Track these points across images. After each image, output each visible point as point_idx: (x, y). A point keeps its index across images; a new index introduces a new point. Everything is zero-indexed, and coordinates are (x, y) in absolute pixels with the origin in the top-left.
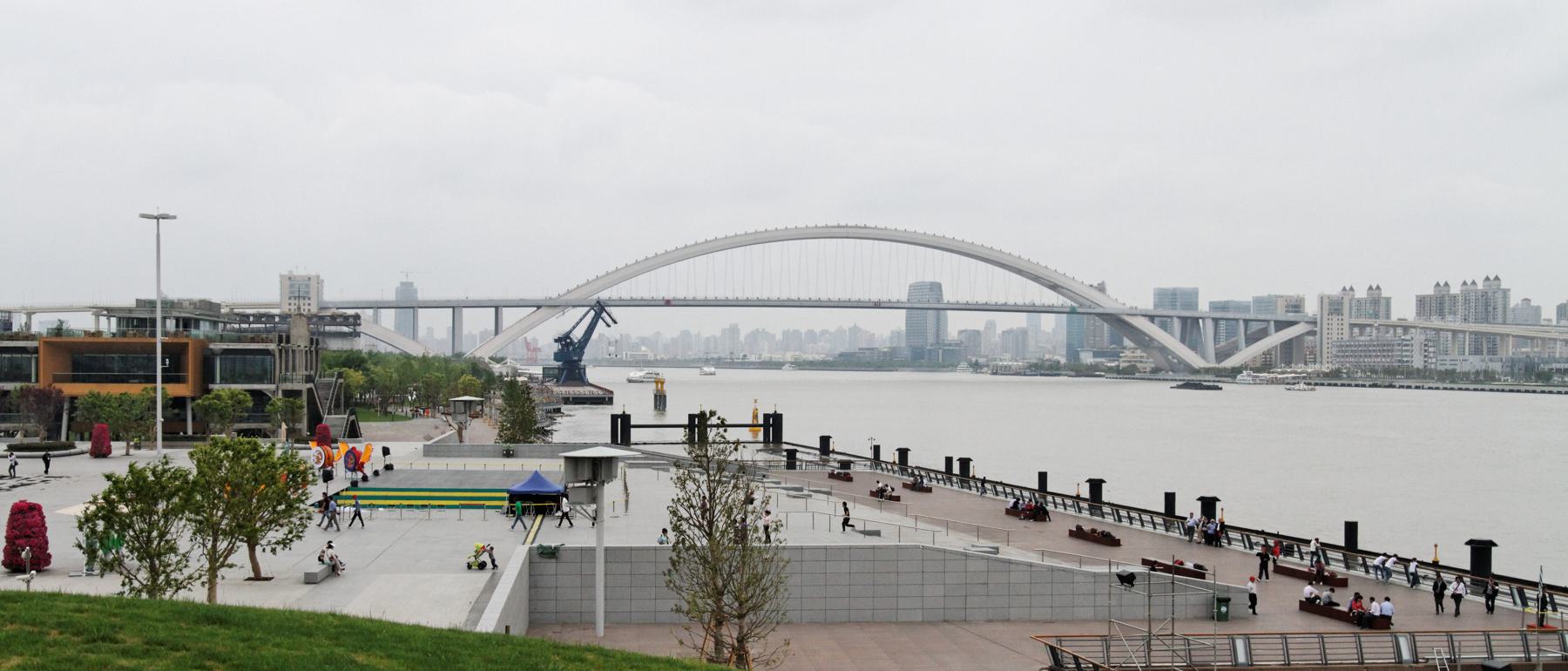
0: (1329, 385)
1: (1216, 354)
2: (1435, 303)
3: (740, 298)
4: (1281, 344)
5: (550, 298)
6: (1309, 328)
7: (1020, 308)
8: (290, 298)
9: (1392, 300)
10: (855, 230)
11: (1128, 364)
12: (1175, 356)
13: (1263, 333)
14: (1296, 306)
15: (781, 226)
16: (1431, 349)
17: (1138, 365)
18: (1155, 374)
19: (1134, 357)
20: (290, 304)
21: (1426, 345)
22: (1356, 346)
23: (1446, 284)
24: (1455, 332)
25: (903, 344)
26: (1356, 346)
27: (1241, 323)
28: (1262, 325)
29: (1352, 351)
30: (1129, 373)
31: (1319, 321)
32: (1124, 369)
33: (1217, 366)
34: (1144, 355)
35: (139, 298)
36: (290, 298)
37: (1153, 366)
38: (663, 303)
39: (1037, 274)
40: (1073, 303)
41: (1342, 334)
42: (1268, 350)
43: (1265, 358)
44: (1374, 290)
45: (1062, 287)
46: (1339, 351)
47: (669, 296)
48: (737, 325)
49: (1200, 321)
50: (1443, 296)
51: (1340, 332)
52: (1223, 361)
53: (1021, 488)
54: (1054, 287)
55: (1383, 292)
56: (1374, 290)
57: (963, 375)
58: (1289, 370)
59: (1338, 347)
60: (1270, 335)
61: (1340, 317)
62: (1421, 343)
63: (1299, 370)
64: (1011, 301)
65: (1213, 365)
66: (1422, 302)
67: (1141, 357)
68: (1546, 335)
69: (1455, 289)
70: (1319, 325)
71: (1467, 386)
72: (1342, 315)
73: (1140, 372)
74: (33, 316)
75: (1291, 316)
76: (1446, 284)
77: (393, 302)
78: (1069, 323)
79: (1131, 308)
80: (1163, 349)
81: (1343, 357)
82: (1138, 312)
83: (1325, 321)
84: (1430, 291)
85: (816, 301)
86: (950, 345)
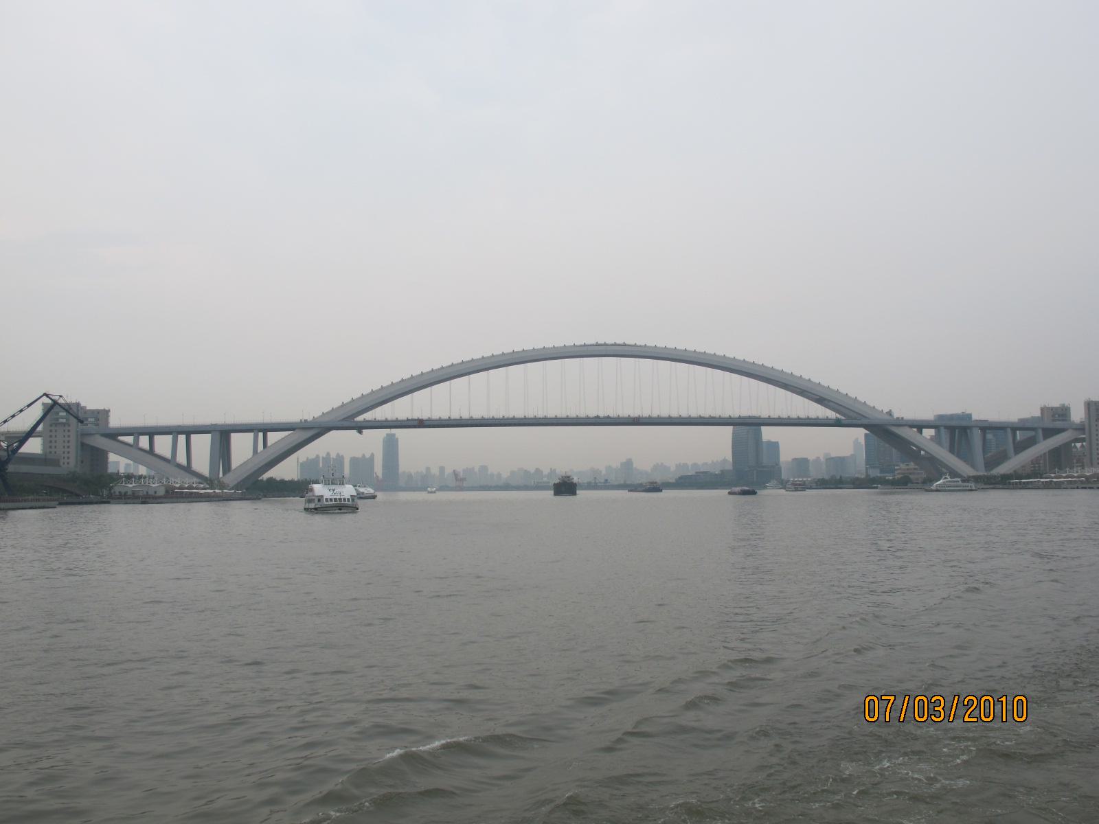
0: (1083, 488)
1: (985, 464)
3: (611, 415)
4: (1050, 451)
5: (306, 421)
8: (51, 426)
11: (901, 476)
13: (1031, 442)
17: (911, 477)
19: (908, 469)
20: (51, 431)
25: (729, 467)
27: (1009, 430)
28: (1031, 434)
31: (1087, 427)
33: (986, 474)
35: (111, 414)
36: (51, 426)
38: (416, 423)
40: (838, 416)
41: (68, 442)
43: (1034, 467)
45: (829, 401)
47: (425, 416)
52: (992, 469)
53: (152, 433)
54: (821, 400)
58: (1064, 475)
60: (1039, 442)
63: (1076, 475)
64: (455, 416)
65: (982, 473)
67: (915, 469)
75: (1059, 424)
78: (734, 433)
79: (898, 418)
85: (605, 418)
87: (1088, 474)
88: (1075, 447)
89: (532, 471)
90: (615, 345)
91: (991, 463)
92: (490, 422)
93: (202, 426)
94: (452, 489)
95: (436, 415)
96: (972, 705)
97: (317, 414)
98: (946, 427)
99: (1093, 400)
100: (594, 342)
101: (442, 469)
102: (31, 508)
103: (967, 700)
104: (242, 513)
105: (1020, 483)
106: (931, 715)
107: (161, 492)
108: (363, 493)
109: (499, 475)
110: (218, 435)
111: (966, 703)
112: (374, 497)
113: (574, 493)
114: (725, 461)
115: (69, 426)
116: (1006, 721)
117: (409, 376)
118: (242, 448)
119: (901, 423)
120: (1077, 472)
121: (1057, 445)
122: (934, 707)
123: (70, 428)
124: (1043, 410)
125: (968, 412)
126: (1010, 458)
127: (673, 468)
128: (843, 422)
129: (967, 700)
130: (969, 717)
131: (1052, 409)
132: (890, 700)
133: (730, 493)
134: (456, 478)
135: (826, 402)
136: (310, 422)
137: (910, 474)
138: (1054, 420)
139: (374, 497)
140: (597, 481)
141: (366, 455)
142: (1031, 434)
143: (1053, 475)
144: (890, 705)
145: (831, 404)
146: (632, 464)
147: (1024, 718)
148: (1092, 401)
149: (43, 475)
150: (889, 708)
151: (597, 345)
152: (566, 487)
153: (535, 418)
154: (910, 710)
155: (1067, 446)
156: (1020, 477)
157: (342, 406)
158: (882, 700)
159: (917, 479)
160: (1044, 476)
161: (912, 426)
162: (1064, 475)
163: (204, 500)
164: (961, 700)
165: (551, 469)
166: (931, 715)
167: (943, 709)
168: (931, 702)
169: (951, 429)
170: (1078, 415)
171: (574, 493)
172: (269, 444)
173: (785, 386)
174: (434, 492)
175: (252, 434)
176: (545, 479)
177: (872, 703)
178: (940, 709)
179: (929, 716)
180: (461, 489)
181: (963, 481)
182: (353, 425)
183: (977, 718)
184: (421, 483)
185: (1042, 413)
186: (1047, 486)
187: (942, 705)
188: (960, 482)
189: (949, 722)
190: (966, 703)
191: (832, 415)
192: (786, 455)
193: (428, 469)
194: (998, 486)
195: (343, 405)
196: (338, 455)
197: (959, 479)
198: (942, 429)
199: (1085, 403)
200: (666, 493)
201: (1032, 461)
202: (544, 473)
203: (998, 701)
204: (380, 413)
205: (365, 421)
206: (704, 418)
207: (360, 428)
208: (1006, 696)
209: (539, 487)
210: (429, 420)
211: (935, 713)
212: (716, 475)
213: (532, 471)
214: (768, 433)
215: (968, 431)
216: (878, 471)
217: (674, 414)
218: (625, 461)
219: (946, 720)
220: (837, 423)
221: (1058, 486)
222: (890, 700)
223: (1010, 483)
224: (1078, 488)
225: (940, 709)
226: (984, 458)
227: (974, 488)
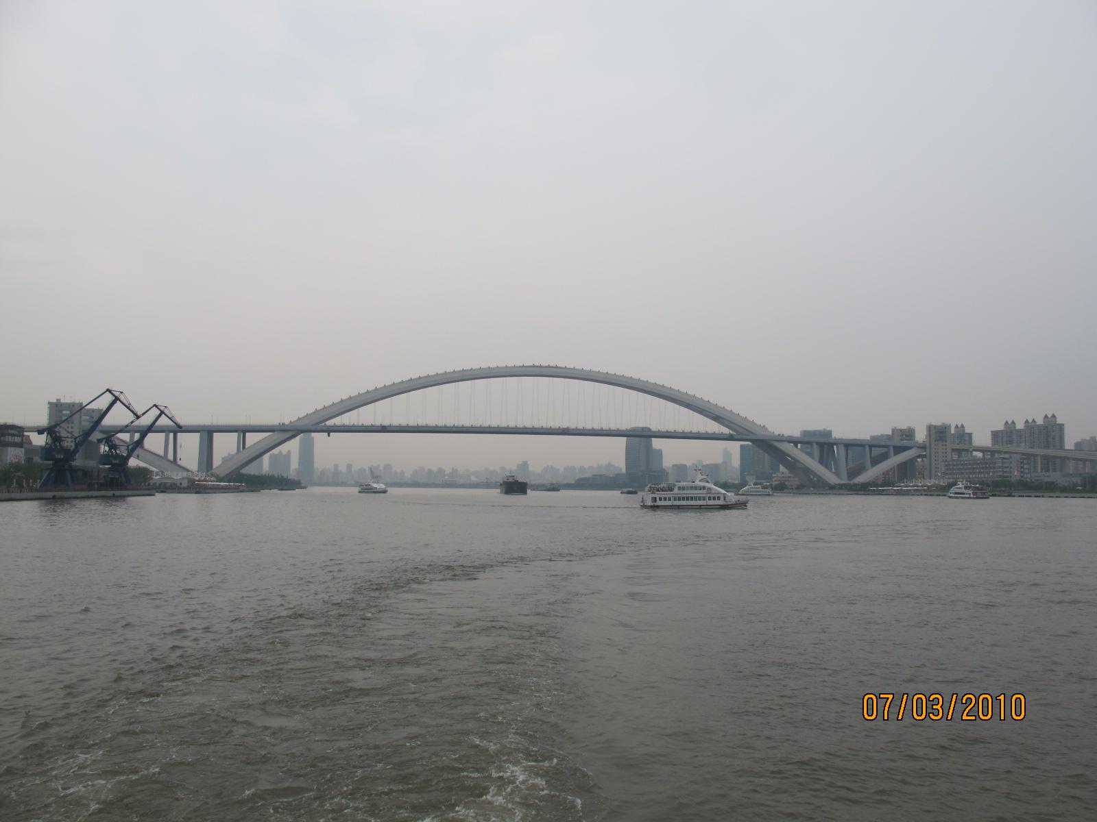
1: (848, 473)
2: (1006, 435)
4: (898, 465)
5: (283, 424)
9: (973, 436)
10: (539, 369)
12: (815, 474)
13: (884, 457)
14: (909, 434)
16: (1026, 466)
17: (787, 483)
18: (800, 489)
21: (1021, 463)
22: (962, 465)
23: (1013, 422)
26: (962, 465)
27: (867, 447)
28: (885, 450)
29: (958, 469)
30: (781, 488)
32: (776, 485)
33: (849, 482)
34: (792, 475)
37: (798, 483)
38: (380, 429)
39: (688, 402)
40: (731, 432)
42: (887, 471)
43: (885, 477)
45: (723, 419)
46: (947, 470)
47: (386, 423)
49: (835, 447)
50: (1012, 431)
51: (945, 455)
52: (852, 479)
54: (716, 418)
55: (1017, 425)
58: (911, 484)
59: (946, 465)
60: (890, 458)
61: (944, 443)
62: (1018, 461)
63: (920, 484)
65: (845, 481)
66: (995, 435)
67: (789, 477)
69: (1020, 426)
71: (823, 492)
72: (946, 441)
73: (788, 489)
75: (906, 443)
76: (1013, 422)
77: (796, 437)
79: (779, 435)
80: (806, 470)
81: (950, 474)
82: (784, 439)
84: (1000, 427)
86: (655, 472)
87: (929, 484)
88: (917, 461)
90: (549, 367)
92: (719, 436)
93: (232, 426)
96: (971, 704)
97: (294, 419)
98: (818, 443)
99: (934, 424)
101: (349, 466)
102: (143, 495)
103: (965, 698)
104: (224, 505)
105: (877, 490)
106: (929, 713)
107: (353, 483)
108: (376, 488)
109: (402, 473)
110: (206, 435)
111: (964, 702)
112: (385, 492)
113: (525, 492)
116: (888, 720)
117: (374, 388)
118: (225, 445)
119: (781, 439)
120: (921, 483)
121: (903, 461)
122: (933, 705)
123: (73, 425)
124: (893, 430)
125: (828, 429)
126: (867, 470)
127: (562, 471)
128: (736, 437)
129: (965, 698)
130: (967, 715)
131: (901, 430)
132: (888, 698)
133: (622, 493)
135: (721, 420)
136: (287, 425)
137: (785, 481)
138: (902, 440)
139: (385, 492)
140: (489, 481)
141: (283, 452)
142: (885, 450)
143: (902, 484)
144: (888, 704)
145: (725, 422)
147: (989, 716)
148: (933, 425)
150: (887, 706)
151: (534, 366)
152: (514, 487)
153: (400, 426)
154: (908, 707)
155: (912, 461)
156: (877, 486)
157: (314, 413)
158: (880, 698)
159: (792, 486)
160: (896, 485)
161: (790, 442)
162: (911, 484)
163: (230, 491)
164: (959, 697)
165: (453, 469)
166: (929, 713)
167: (941, 707)
168: (929, 701)
169: (821, 445)
170: (921, 436)
171: (525, 492)
172: (247, 446)
173: (688, 406)
175: (236, 434)
176: (446, 477)
177: (985, 701)
178: (938, 707)
179: (928, 714)
181: (763, 488)
182: (324, 428)
183: (976, 716)
184: (334, 479)
185: (893, 434)
186: (899, 493)
187: (941, 703)
188: (760, 489)
189: (947, 720)
190: (964, 702)
191: (726, 431)
192: (668, 462)
193: (336, 466)
194: (860, 492)
195: (316, 411)
197: (760, 486)
198: (815, 444)
199: (927, 426)
200: (563, 493)
201: (883, 474)
202: (446, 472)
203: (997, 699)
205: (335, 426)
206: (374, 426)
207: (329, 431)
208: (1004, 694)
209: (487, 485)
210: (390, 426)
211: (933, 711)
212: (611, 478)
214: (657, 443)
217: (605, 427)
218: (521, 463)
219: (944, 718)
220: (730, 438)
221: (907, 493)
222: (888, 698)
223: (869, 490)
224: (921, 495)
225: (938, 707)
227: (771, 493)
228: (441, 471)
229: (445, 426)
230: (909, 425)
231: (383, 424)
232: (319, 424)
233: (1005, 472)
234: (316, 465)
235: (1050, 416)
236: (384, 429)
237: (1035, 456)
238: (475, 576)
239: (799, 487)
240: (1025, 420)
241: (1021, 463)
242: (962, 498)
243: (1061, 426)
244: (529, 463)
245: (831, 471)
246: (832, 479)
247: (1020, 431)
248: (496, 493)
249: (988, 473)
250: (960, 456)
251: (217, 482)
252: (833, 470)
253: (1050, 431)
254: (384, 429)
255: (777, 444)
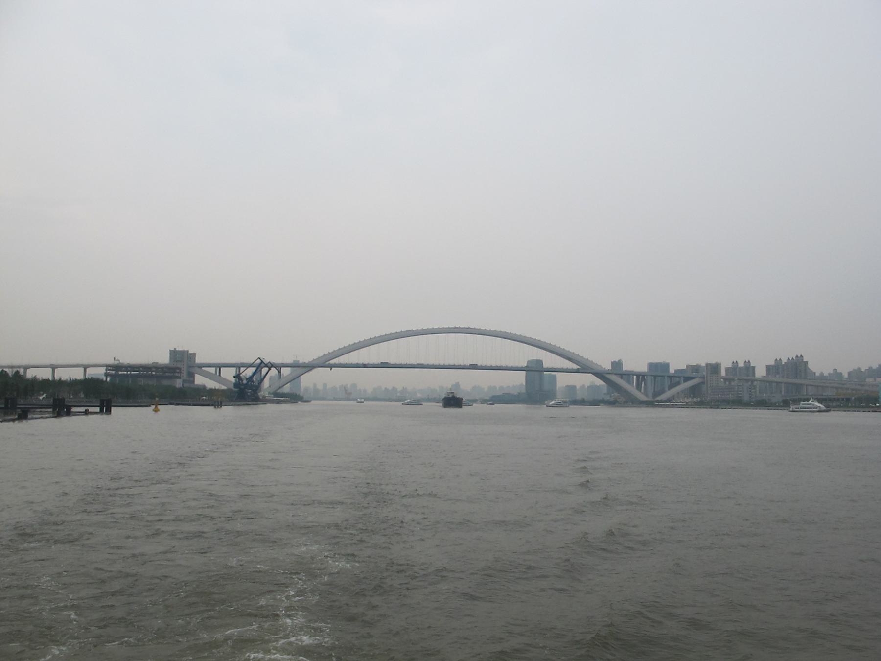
2: (774, 369)
5: (305, 363)
6: (701, 380)
7: (484, 368)
10: (455, 329)
13: (678, 383)
15: (394, 332)
17: (618, 400)
24: (777, 383)
25: (524, 391)
40: (578, 367)
44: (748, 363)
47: (366, 362)
48: (458, 383)
53: (219, 367)
54: (569, 359)
55: (751, 364)
56: (748, 363)
57: (488, 398)
65: (650, 399)
66: (768, 368)
68: (824, 385)
70: (706, 379)
74: (56, 370)
76: (780, 360)
80: (626, 391)
83: (709, 378)
89: (390, 388)
91: (655, 394)
94: (341, 399)
95: (371, 362)
98: (636, 375)
100: (453, 326)
109: (365, 391)
114: (522, 385)
115: (183, 362)
127: (486, 389)
128: (580, 371)
134: (346, 393)
146: (459, 386)
149: (711, 408)
152: (453, 401)
174: (363, 402)
176: (399, 394)
180: (348, 399)
185: (687, 368)
191: (575, 367)
193: (315, 385)
196: (386, 388)
202: (398, 390)
204: (343, 360)
205: (335, 364)
207: (331, 367)
210: (368, 364)
212: (515, 395)
213: (390, 388)
215: (645, 377)
216: (90, 411)
217: (504, 365)
220: (577, 371)
226: (804, 384)
228: (394, 389)
229: (401, 364)
230: (697, 363)
231: (364, 363)
232: (325, 363)
233: (740, 394)
234: (302, 384)
235: (799, 356)
236: (364, 366)
237: (781, 383)
238: (421, 403)
239: (626, 402)
240: (775, 359)
241: (750, 388)
242: (810, 411)
243: (754, 368)
244: (460, 383)
245: (640, 391)
246: (642, 397)
247: (740, 368)
248: (438, 407)
249: (729, 394)
250: (730, 383)
251: (274, 397)
252: (642, 391)
253: (798, 366)
254: (364, 366)
255: (608, 376)
